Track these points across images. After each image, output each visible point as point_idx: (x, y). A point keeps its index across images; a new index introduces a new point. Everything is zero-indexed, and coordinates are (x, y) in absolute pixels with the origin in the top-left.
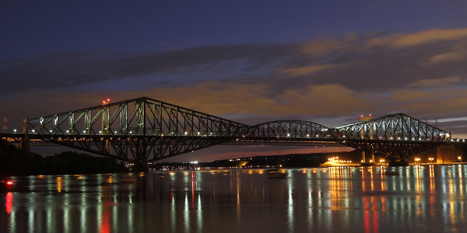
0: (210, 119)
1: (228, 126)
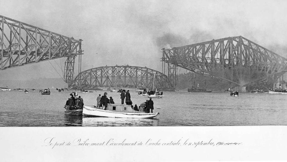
0: (39, 33)
1: (58, 41)
